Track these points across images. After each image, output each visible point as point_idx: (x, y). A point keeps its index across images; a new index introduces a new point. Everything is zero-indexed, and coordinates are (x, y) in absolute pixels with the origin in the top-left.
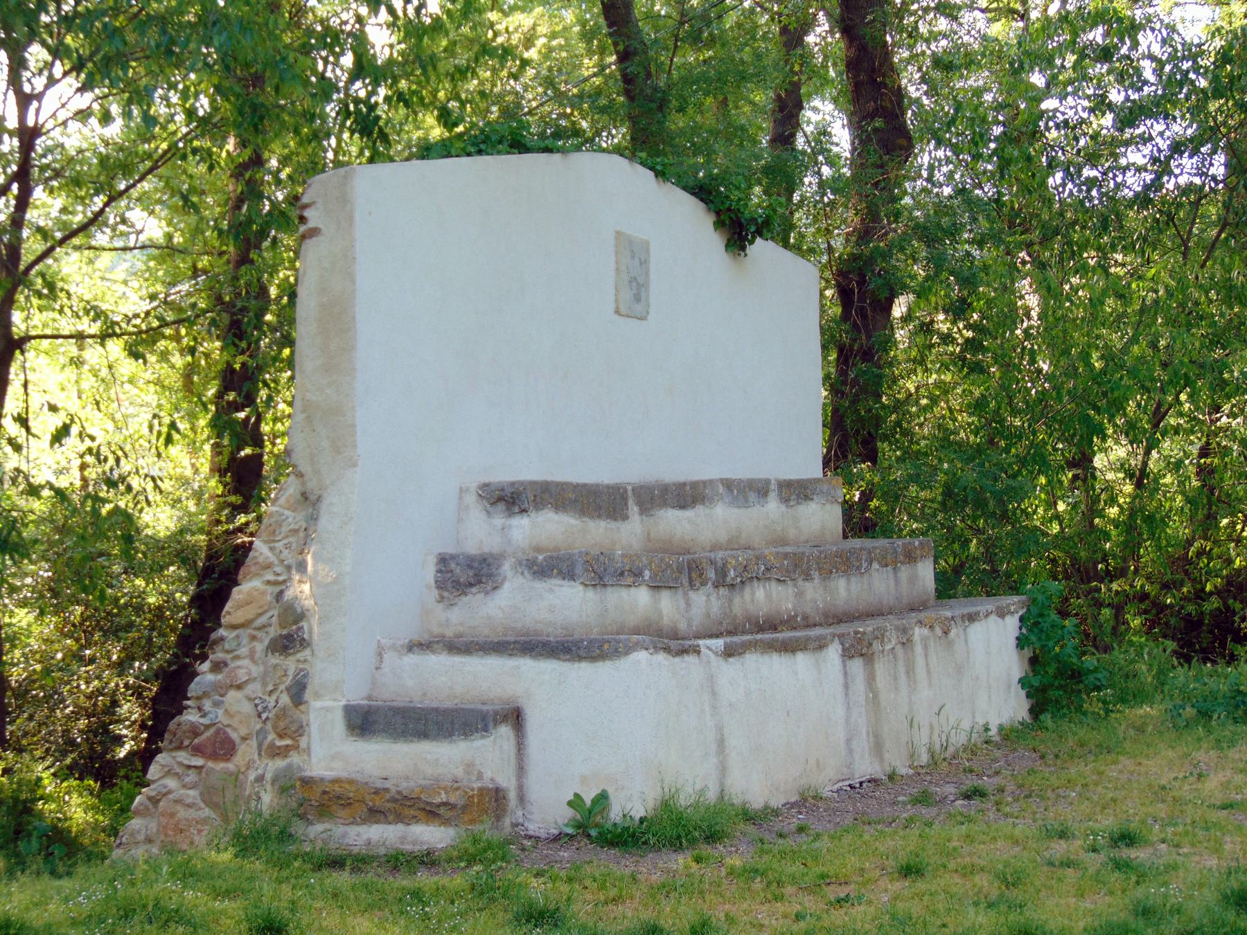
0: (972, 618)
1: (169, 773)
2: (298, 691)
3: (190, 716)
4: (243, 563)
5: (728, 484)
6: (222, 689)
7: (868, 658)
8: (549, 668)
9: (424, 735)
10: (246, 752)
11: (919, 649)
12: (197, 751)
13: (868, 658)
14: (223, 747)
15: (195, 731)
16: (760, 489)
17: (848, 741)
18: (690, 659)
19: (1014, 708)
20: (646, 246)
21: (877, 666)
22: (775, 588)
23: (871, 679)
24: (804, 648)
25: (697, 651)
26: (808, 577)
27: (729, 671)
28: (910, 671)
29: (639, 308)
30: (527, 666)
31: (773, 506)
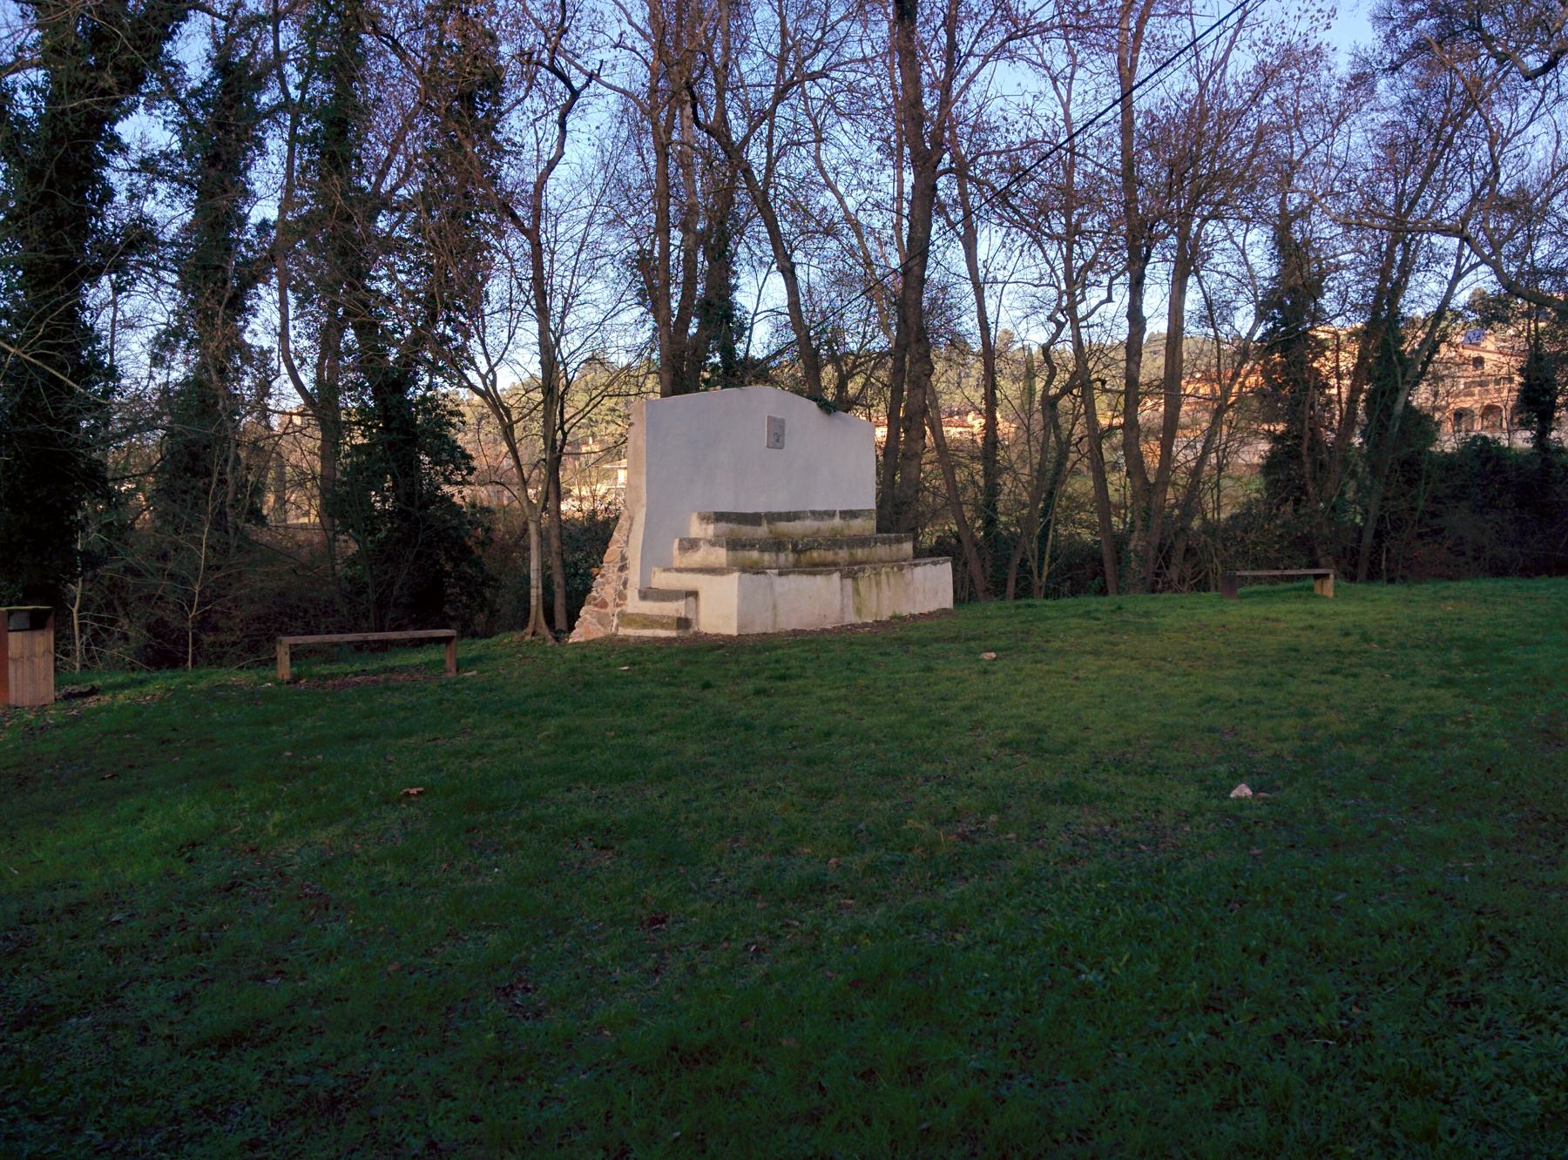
0: (916, 565)
1: (587, 613)
2: (625, 584)
3: (594, 594)
4: (794, 630)
5: (813, 513)
6: (604, 584)
7: (855, 579)
8: (708, 577)
9: (663, 600)
10: (611, 605)
11: (883, 577)
12: (596, 605)
13: (855, 579)
14: (604, 605)
15: (595, 599)
16: (831, 514)
17: (842, 609)
18: (762, 576)
19: (948, 602)
20: (783, 421)
21: (860, 583)
22: (822, 552)
23: (857, 591)
24: (820, 573)
25: (766, 573)
26: (841, 548)
27: (779, 581)
28: (878, 584)
29: (778, 445)
30: (701, 577)
31: (837, 521)
